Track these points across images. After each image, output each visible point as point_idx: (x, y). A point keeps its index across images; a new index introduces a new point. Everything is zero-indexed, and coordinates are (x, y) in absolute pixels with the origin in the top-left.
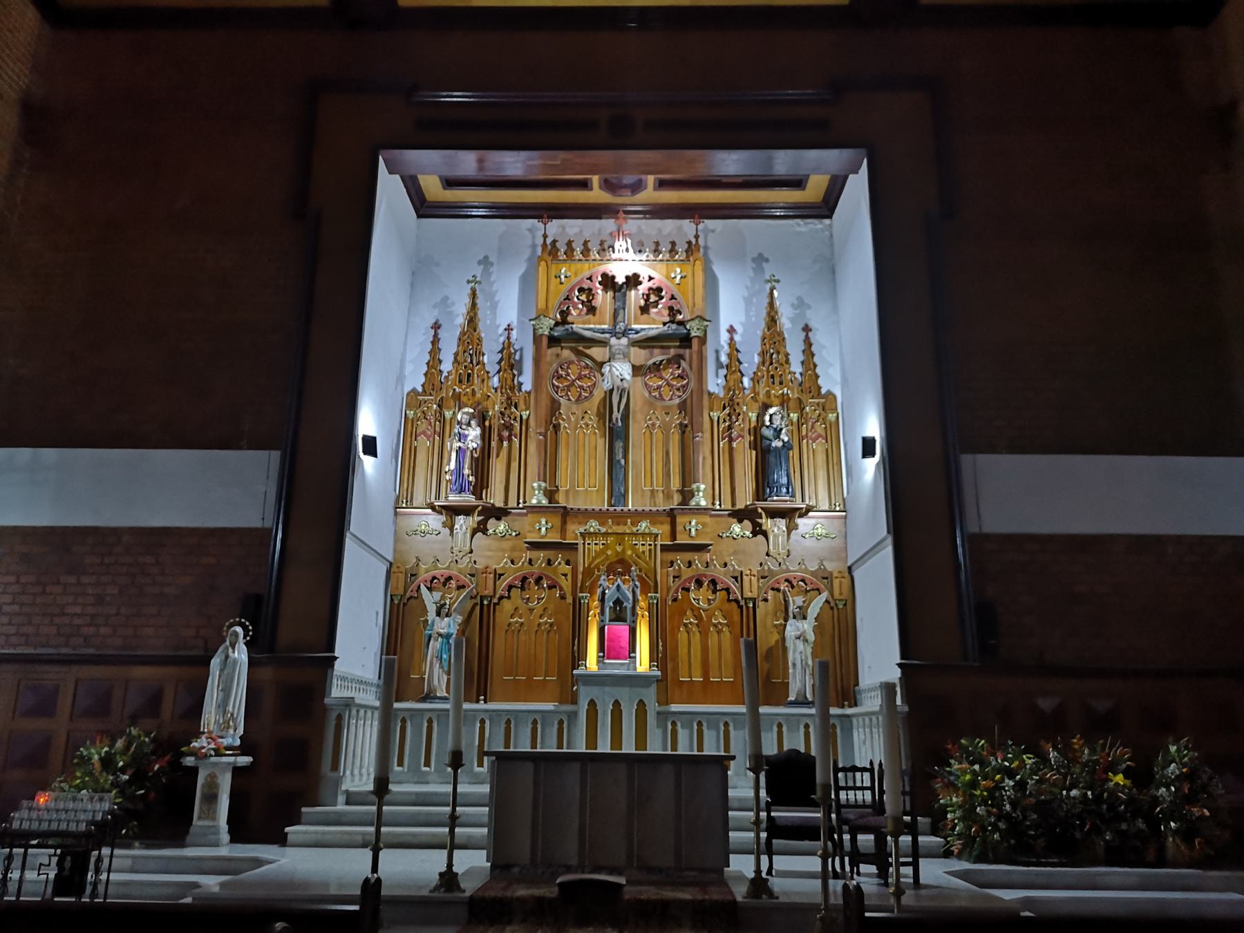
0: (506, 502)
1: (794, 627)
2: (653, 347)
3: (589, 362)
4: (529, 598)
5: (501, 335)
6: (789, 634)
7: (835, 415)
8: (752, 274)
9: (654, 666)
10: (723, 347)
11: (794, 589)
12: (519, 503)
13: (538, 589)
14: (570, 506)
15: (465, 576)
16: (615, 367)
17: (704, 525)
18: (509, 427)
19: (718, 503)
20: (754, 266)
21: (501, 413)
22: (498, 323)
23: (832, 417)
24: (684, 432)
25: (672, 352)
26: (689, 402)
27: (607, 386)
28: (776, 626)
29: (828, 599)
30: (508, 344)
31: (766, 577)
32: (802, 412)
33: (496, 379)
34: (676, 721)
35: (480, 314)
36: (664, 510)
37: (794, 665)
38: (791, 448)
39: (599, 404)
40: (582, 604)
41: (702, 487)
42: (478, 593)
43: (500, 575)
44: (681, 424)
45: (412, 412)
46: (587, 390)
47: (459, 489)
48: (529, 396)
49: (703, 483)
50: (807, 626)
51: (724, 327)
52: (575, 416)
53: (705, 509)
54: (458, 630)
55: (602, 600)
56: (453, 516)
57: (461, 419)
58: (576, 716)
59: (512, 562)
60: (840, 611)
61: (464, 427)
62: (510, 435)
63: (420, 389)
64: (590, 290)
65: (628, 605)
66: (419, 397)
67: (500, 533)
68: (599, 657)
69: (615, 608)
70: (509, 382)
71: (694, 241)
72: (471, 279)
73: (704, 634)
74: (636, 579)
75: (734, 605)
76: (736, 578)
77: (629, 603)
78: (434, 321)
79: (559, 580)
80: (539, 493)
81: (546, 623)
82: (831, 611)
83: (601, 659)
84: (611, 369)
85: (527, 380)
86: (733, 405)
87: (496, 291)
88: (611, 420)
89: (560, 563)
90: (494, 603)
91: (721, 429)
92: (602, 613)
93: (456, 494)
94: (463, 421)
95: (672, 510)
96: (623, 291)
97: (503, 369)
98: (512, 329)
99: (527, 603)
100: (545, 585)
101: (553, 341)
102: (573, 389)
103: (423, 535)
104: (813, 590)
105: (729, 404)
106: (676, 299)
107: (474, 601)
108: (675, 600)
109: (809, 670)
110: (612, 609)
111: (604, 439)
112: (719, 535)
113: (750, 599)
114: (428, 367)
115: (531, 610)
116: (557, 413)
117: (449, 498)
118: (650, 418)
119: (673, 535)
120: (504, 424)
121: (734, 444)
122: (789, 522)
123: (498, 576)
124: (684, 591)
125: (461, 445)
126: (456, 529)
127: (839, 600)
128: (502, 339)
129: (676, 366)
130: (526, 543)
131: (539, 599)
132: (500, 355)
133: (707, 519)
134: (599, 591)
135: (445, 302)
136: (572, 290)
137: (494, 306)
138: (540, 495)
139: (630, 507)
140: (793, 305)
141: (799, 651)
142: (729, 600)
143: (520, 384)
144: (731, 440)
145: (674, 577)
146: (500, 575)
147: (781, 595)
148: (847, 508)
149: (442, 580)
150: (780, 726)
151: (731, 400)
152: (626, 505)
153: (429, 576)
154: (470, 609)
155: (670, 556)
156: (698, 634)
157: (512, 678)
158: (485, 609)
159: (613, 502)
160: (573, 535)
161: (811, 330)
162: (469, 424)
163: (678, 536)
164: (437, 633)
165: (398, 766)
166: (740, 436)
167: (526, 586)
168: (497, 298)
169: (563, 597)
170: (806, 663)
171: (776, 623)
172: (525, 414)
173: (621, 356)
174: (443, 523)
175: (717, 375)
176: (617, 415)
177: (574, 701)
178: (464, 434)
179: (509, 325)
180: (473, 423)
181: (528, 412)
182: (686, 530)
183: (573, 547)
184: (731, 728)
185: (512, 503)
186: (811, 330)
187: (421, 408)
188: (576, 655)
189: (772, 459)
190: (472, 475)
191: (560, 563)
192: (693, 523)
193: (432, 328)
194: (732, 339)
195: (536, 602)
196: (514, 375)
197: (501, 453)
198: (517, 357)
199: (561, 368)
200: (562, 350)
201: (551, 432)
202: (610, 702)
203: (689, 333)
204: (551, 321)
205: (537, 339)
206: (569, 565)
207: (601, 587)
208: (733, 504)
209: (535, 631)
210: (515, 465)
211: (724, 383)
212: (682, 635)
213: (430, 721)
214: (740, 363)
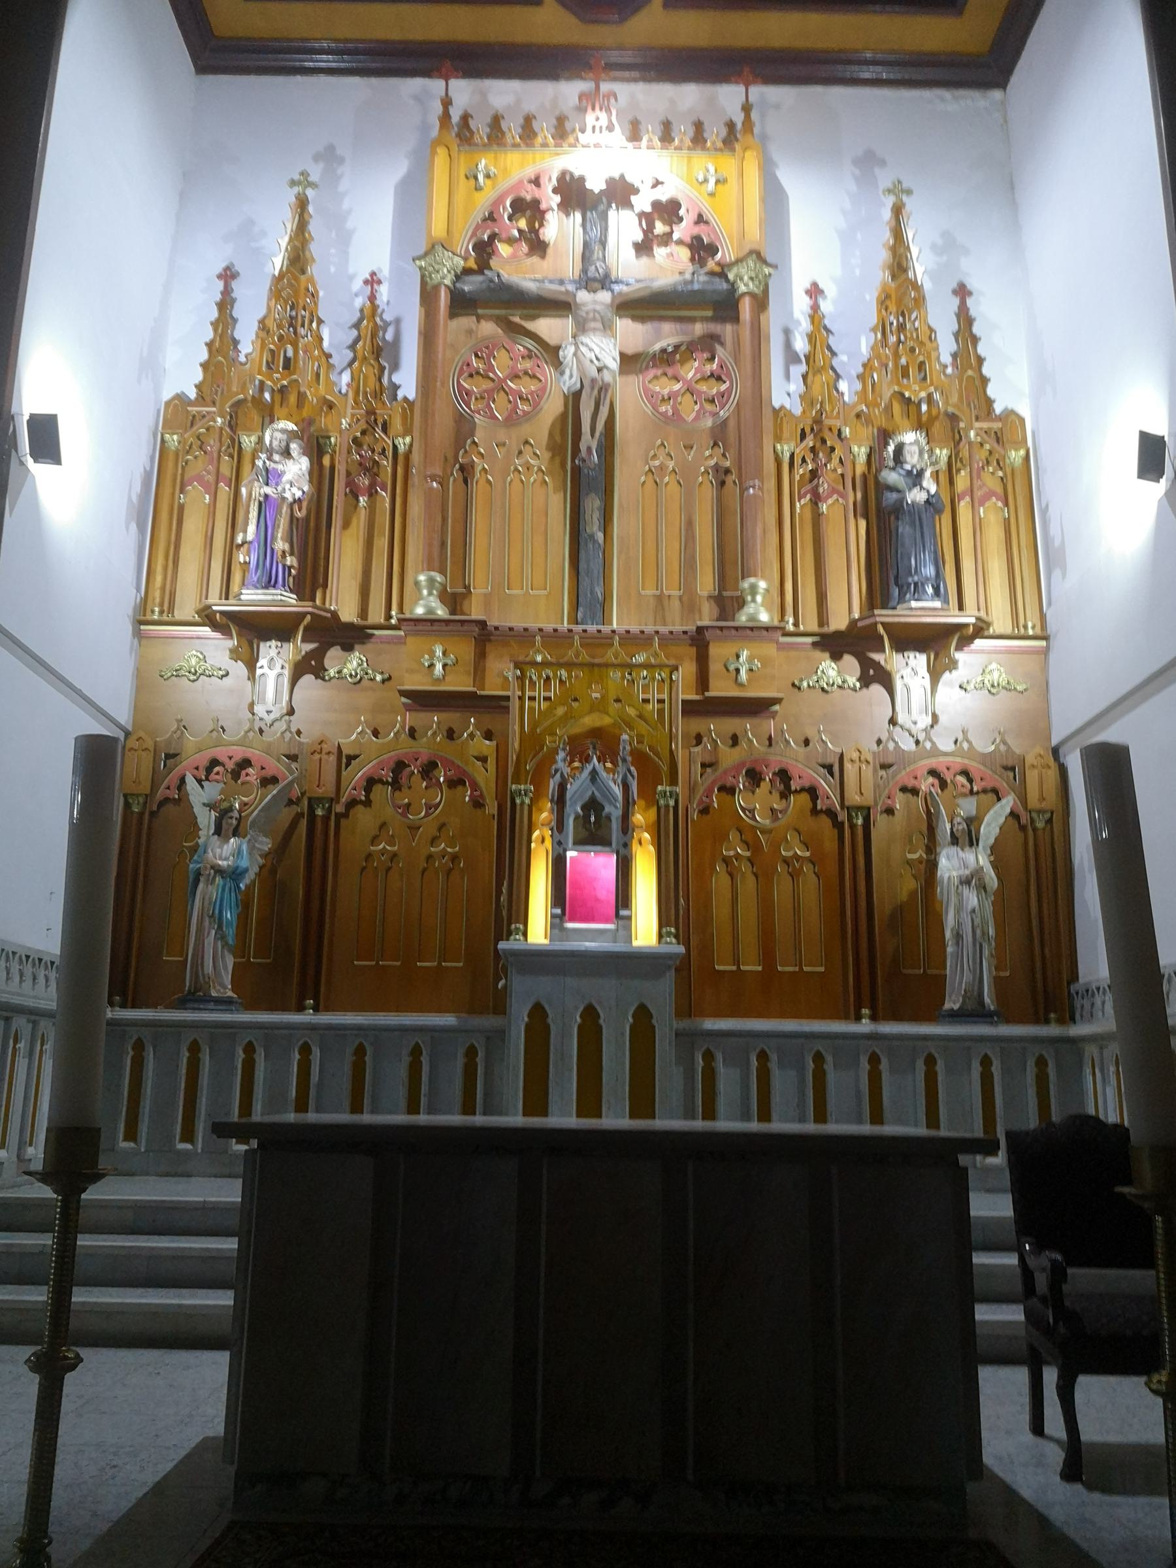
0: (363, 613)
1: (955, 862)
2: (662, 319)
3: (529, 343)
4: (409, 805)
5: (356, 295)
6: (946, 876)
7: (1022, 452)
8: (853, 187)
9: (669, 934)
10: (799, 323)
11: (946, 791)
12: (388, 617)
13: (426, 788)
14: (493, 622)
15: (279, 760)
16: (587, 346)
17: (765, 662)
18: (371, 469)
19: (791, 620)
20: (857, 172)
21: (355, 440)
22: (351, 270)
23: (1015, 456)
24: (723, 483)
25: (699, 329)
26: (732, 424)
27: (569, 381)
28: (909, 863)
29: (1016, 811)
30: (372, 309)
31: (890, 766)
32: (957, 444)
33: (346, 378)
34: (712, 1049)
35: (314, 248)
36: (685, 633)
37: (958, 936)
38: (939, 511)
39: (553, 425)
40: (518, 807)
41: (762, 585)
42: (303, 794)
43: (351, 758)
44: (716, 468)
45: (175, 437)
46: (527, 399)
47: (265, 579)
48: (412, 411)
49: (763, 577)
50: (979, 858)
51: (799, 286)
52: (503, 450)
53: (767, 629)
54: (261, 868)
55: (560, 802)
56: (255, 641)
57: (271, 442)
58: (503, 1040)
59: (376, 733)
60: (1040, 833)
61: (276, 457)
62: (373, 485)
63: (192, 394)
64: (536, 203)
65: (614, 811)
66: (189, 408)
67: (351, 675)
68: (553, 916)
69: (586, 817)
70: (372, 381)
71: (739, 119)
72: (297, 177)
73: (764, 876)
74: (629, 759)
75: (826, 821)
76: (829, 768)
77: (616, 807)
78: (224, 265)
79: (469, 769)
80: (430, 594)
81: (443, 854)
82: (1021, 835)
83: (557, 920)
84: (577, 348)
85: (407, 381)
86: (820, 430)
87: (349, 212)
88: (576, 450)
89: (472, 736)
90: (336, 814)
91: (797, 478)
92: (560, 826)
93: (257, 588)
94: (275, 443)
95: (700, 630)
96: (602, 207)
97: (359, 354)
98: (379, 282)
99: (404, 815)
100: (442, 779)
101: (461, 304)
102: (500, 397)
103: (192, 677)
104: (985, 791)
105: (812, 429)
106: (707, 223)
107: (295, 809)
108: (705, 811)
109: (990, 944)
110: (581, 821)
111: (562, 494)
112: (793, 685)
113: (859, 808)
114: (210, 352)
115: (414, 828)
116: (469, 441)
117: (243, 597)
118: (655, 455)
119: (703, 681)
120: (360, 464)
121: (824, 508)
122: (935, 659)
123: (346, 760)
124: (724, 794)
125: (268, 490)
126: (261, 667)
127: (1039, 812)
128: (359, 302)
129: (706, 355)
130: (403, 693)
131: (429, 807)
132: (355, 333)
133: (770, 650)
134: (553, 784)
135: (247, 231)
136: (499, 201)
137: (344, 239)
138: (431, 598)
139: (615, 626)
140: (934, 247)
141: (970, 908)
142: (815, 811)
143: (396, 387)
144: (816, 499)
145: (704, 765)
146: (351, 758)
147: (920, 802)
148: (1052, 627)
149: (230, 765)
150: (930, 1061)
151: (818, 421)
152: (605, 619)
153: (203, 759)
154: (287, 825)
155: (698, 725)
156: (751, 880)
157: (374, 963)
158: (319, 825)
159: (580, 615)
160: (499, 681)
161: (970, 294)
162: (287, 453)
163: (713, 682)
164: (212, 867)
165: (126, 1139)
166: (834, 491)
167: (404, 780)
168: (350, 224)
169: (478, 804)
170: (985, 933)
171: (910, 856)
172: (403, 443)
173: (599, 325)
174: (231, 651)
175: (787, 376)
176: (589, 442)
177: (499, 1005)
178: (275, 470)
179: (373, 274)
180: (294, 447)
181: (408, 439)
182: (728, 670)
183: (498, 705)
184: (829, 1066)
185: (376, 615)
186: (970, 294)
187: (195, 428)
188: (504, 913)
189: (905, 529)
190: (292, 554)
191: (472, 736)
192: (743, 658)
193: (220, 277)
194: (815, 308)
195: (423, 813)
196: (382, 369)
197: (354, 521)
198: (389, 336)
199: (476, 356)
200: (478, 321)
201: (454, 481)
202: (576, 1008)
203: (733, 287)
204: (456, 259)
205: (428, 295)
206: (490, 740)
207: (558, 775)
208: (822, 620)
209: (421, 868)
210: (381, 543)
211: (802, 388)
212: (720, 880)
213: (194, 1048)
214: (834, 354)
